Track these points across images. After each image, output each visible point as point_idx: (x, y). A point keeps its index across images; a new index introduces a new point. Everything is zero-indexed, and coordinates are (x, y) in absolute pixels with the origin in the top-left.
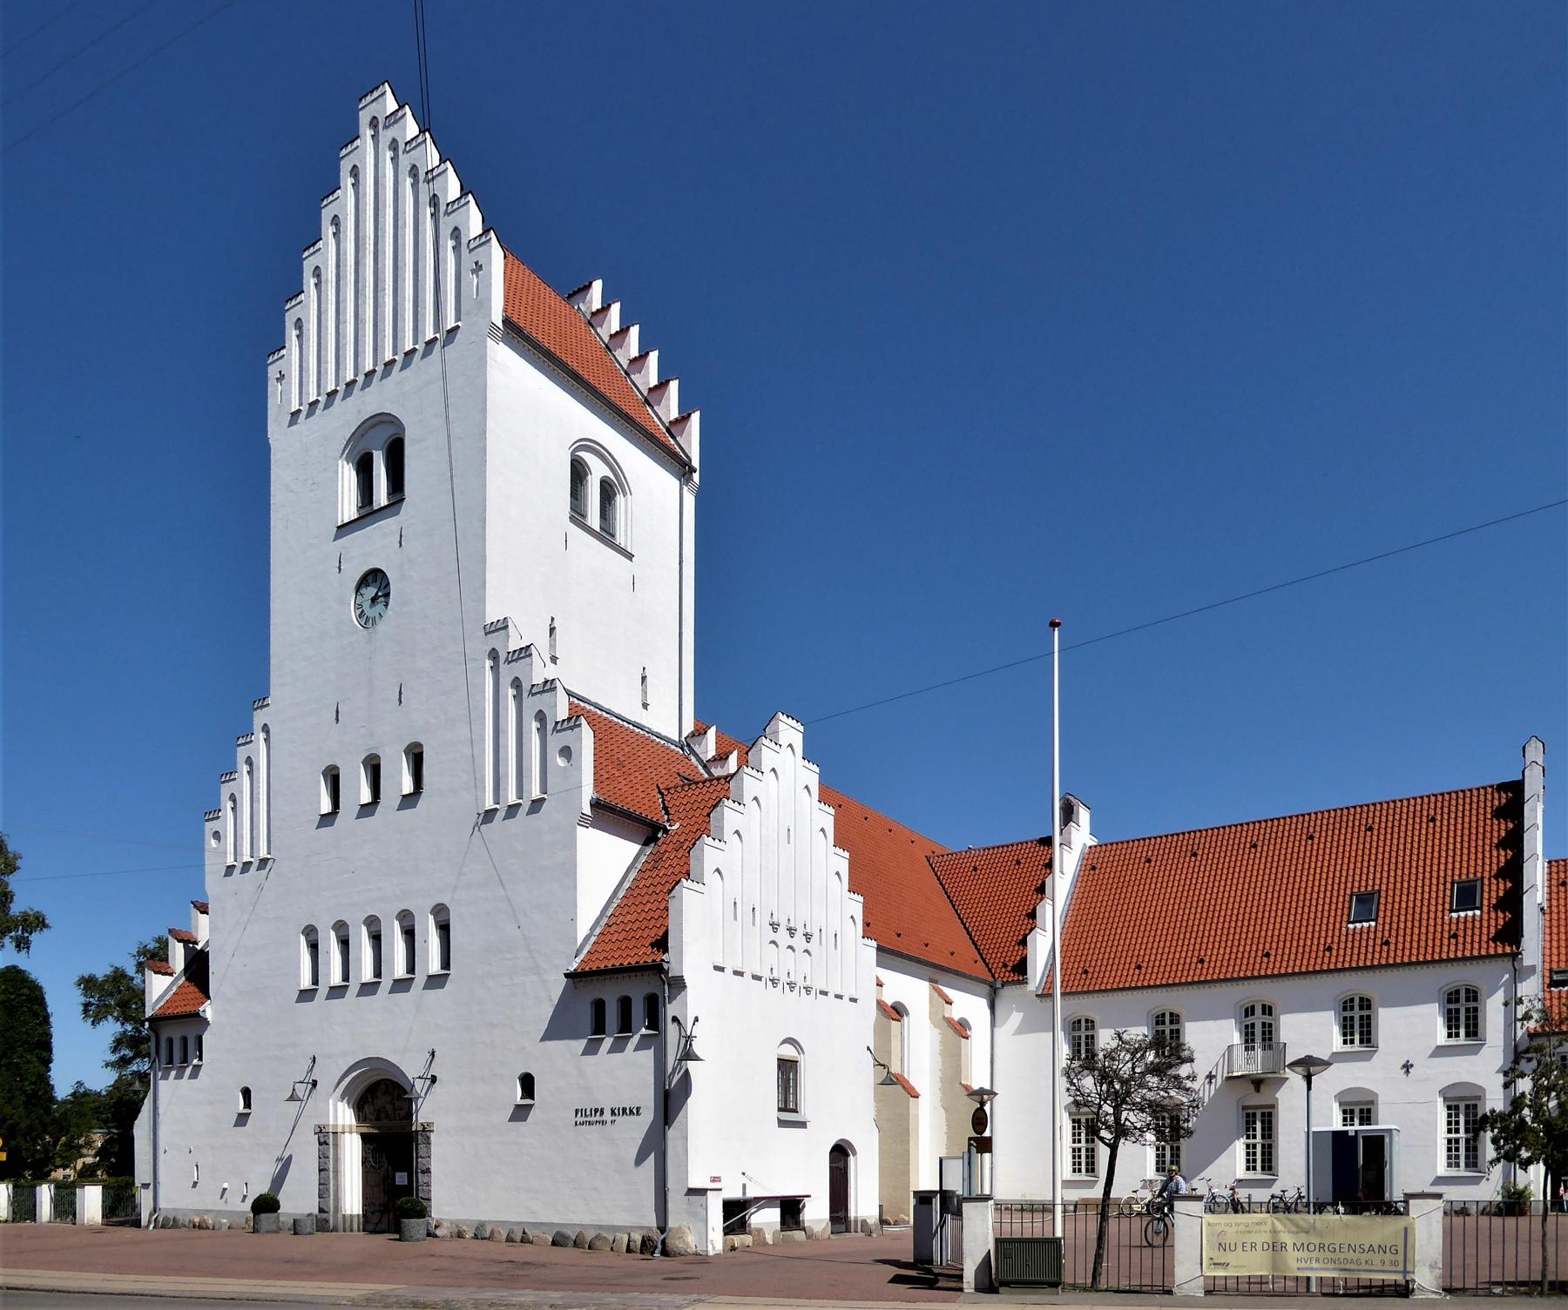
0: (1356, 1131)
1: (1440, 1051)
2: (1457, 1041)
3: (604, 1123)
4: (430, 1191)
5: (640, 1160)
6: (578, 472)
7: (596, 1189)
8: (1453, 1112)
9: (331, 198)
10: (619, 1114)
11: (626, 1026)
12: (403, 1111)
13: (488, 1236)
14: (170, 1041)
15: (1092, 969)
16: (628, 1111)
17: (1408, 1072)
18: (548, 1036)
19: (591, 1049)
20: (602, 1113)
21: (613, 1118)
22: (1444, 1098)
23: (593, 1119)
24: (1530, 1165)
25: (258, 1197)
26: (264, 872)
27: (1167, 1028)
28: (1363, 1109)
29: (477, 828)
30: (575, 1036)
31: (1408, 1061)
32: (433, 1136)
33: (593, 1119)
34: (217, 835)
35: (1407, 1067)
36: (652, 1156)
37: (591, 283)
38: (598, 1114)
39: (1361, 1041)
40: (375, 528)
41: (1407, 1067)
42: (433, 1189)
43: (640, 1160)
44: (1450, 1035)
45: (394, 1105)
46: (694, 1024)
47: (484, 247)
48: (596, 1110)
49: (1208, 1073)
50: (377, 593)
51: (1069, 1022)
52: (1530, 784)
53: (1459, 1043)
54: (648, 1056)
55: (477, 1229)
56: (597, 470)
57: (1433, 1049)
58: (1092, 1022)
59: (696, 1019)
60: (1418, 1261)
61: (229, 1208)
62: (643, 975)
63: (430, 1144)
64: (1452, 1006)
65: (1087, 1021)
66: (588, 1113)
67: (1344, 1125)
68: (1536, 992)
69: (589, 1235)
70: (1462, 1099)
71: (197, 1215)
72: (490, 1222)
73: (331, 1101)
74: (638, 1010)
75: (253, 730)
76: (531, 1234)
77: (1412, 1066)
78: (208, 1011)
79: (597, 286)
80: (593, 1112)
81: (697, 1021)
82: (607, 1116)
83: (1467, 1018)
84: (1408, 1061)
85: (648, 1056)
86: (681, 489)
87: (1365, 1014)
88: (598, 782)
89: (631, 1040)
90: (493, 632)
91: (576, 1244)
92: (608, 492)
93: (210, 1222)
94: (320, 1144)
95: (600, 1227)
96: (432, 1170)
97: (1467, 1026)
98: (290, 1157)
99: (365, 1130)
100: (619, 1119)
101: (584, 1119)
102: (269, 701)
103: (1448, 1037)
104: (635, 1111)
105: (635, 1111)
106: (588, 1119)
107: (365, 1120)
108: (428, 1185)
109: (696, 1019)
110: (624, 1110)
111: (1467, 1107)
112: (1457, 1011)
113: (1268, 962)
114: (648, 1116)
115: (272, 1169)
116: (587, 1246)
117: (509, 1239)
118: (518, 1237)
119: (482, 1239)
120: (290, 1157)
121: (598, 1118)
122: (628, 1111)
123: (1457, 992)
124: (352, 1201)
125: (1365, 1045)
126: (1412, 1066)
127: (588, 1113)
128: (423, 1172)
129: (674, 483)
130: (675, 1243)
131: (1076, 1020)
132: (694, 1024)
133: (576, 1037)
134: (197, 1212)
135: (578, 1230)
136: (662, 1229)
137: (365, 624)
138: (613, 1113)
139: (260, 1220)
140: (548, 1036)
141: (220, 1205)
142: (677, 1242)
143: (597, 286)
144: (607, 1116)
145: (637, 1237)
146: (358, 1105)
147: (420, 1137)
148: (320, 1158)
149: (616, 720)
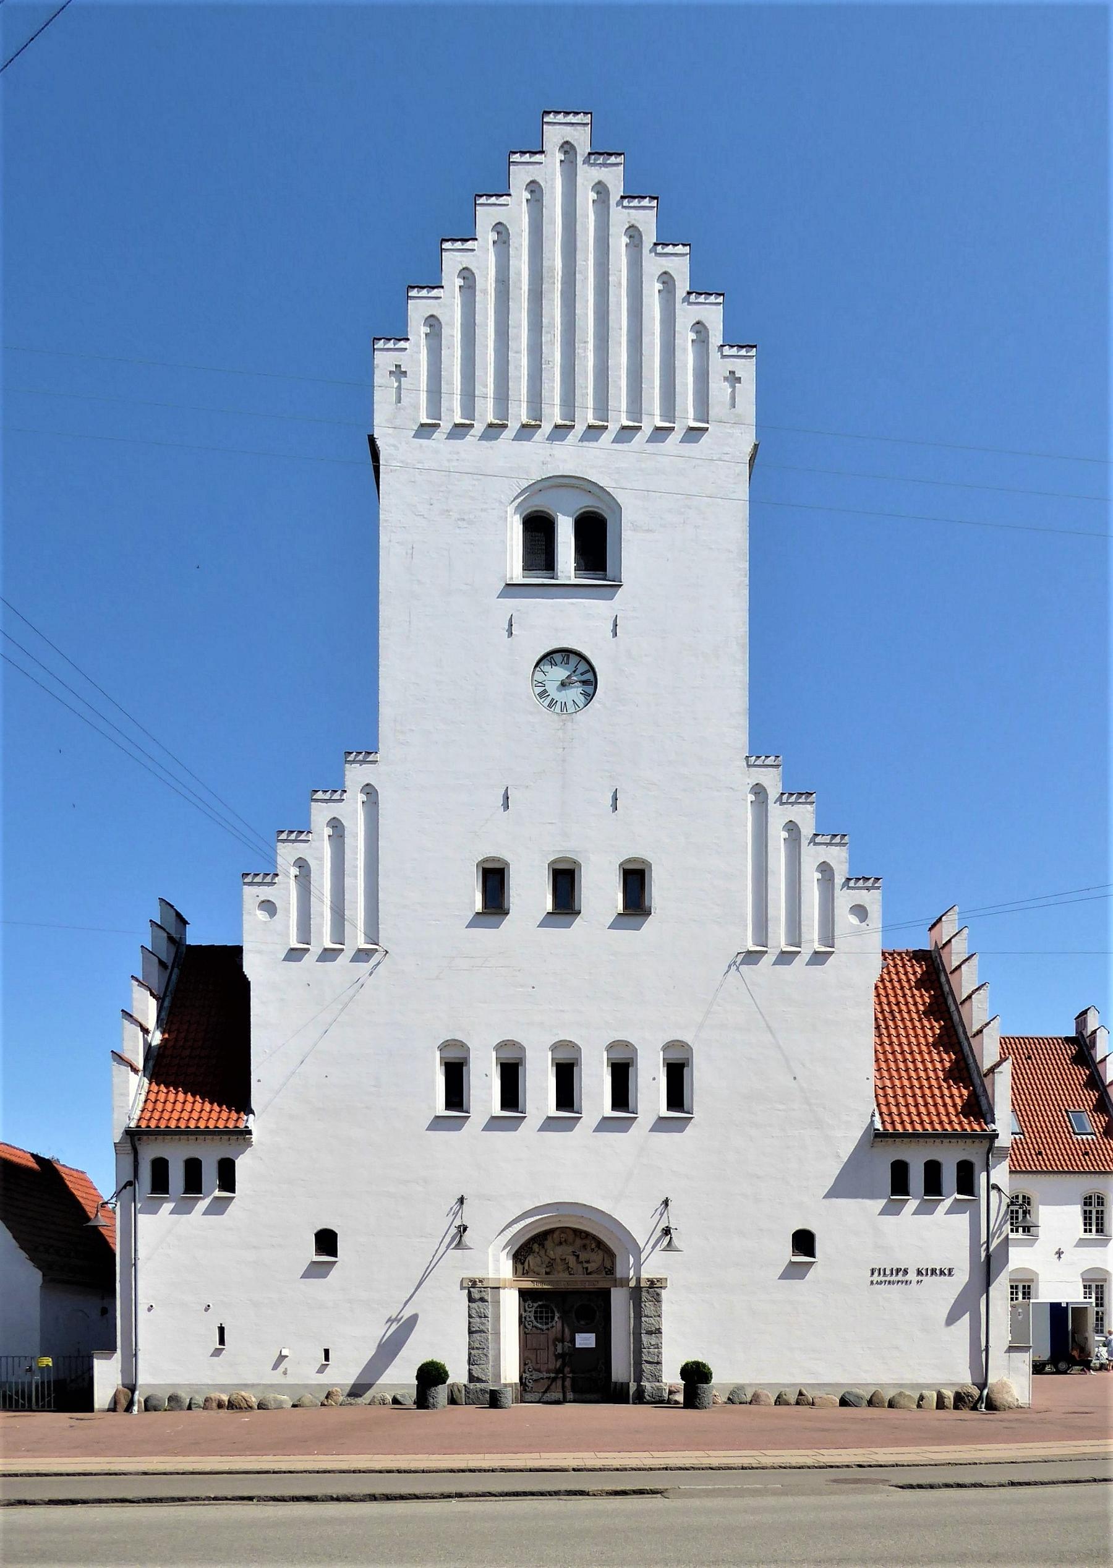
0: (1067, 1303)
1: (1082, 1243)
2: (1016, 1235)
4: (660, 1353)
5: (951, 1319)
7: (897, 1348)
8: (1087, 1290)
9: (493, 200)
10: (927, 1274)
11: (933, 1187)
12: (593, 1264)
13: (749, 1400)
16: (938, 1272)
17: (1060, 1257)
18: (834, 1192)
19: (894, 1209)
20: (906, 1272)
21: (920, 1278)
22: (1083, 1279)
23: (894, 1278)
25: (421, 1366)
26: (365, 967)
28: (1025, 1286)
29: (734, 968)
30: (873, 1196)
31: (1060, 1249)
32: (664, 1294)
33: (894, 1278)
34: (269, 907)
35: (1059, 1254)
36: (967, 1315)
38: (901, 1274)
39: (1097, 1231)
40: (573, 604)
41: (1059, 1254)
42: (664, 1350)
43: (951, 1319)
44: (1085, 1231)
47: (743, 360)
48: (898, 1271)
49: (1057, 1250)
50: (569, 677)
52: (1101, 1043)
53: (1017, 1237)
54: (962, 1220)
55: (731, 1394)
57: (1077, 1240)
58: (1029, 1198)
61: (290, 1380)
62: (974, 1142)
63: (659, 1301)
64: (1088, 1208)
66: (888, 1272)
67: (1085, 1298)
69: (888, 1394)
70: (1021, 1281)
71: (223, 1392)
72: (750, 1385)
73: (490, 1250)
74: (949, 1177)
75: (343, 783)
76: (809, 1394)
77: (1063, 1252)
78: (252, 1125)
80: (894, 1272)
82: (912, 1276)
83: (1097, 1218)
84: (1060, 1249)
85: (962, 1220)
87: (1100, 1209)
89: (942, 1203)
90: (759, 766)
91: (870, 1403)
93: (254, 1399)
94: (471, 1299)
95: (901, 1385)
96: (663, 1331)
97: (1097, 1225)
98: (414, 1318)
99: (527, 1285)
100: (927, 1280)
101: (882, 1278)
102: (378, 757)
103: (1085, 1232)
104: (946, 1272)
105: (946, 1272)
106: (888, 1279)
107: (525, 1273)
108: (658, 1346)
110: (933, 1271)
111: (1097, 1286)
112: (1090, 1212)
114: (962, 1277)
115: (378, 1331)
116: (886, 1405)
117: (780, 1401)
118: (793, 1398)
119: (741, 1403)
120: (414, 1318)
121: (900, 1277)
122: (938, 1272)
123: (1090, 1197)
124: (510, 1371)
125: (1026, 1233)
126: (1063, 1252)
127: (888, 1272)
128: (650, 1333)
130: (1000, 1398)
133: (872, 1196)
134: (222, 1388)
135: (873, 1390)
136: (982, 1386)
137: (579, 707)
138: (919, 1272)
139: (437, 1393)
140: (834, 1192)
141: (276, 1378)
142: (1006, 1396)
144: (912, 1276)
145: (949, 1394)
147: (644, 1294)
148: (470, 1316)
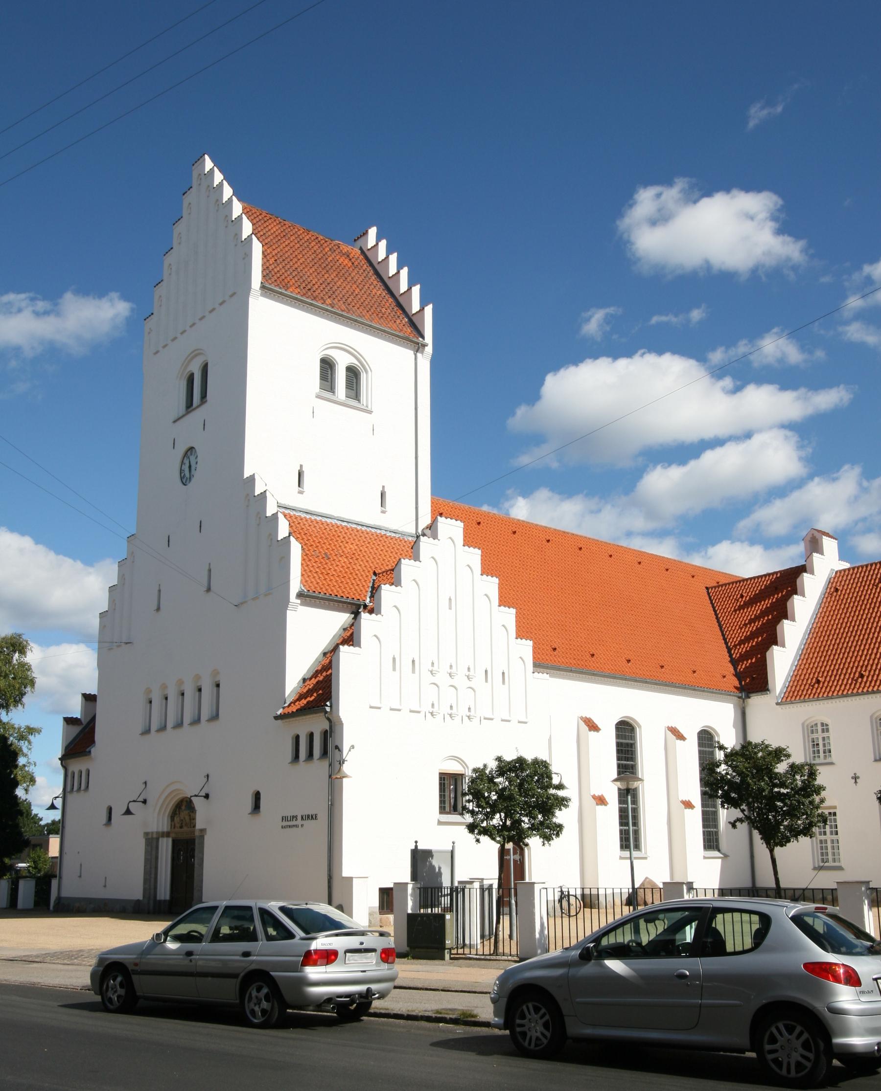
3: (296, 826)
6: (327, 366)
14: (74, 773)
15: (867, 672)
17: (856, 782)
21: (303, 822)
24: (20, 834)
27: (820, 735)
35: (855, 778)
37: (367, 231)
43: (440, 868)
45: (190, 815)
46: (350, 750)
51: (876, 718)
56: (342, 362)
58: (827, 725)
59: (353, 747)
60: (736, 921)
65: (822, 724)
68: (82, 792)
79: (373, 232)
81: (353, 748)
86: (416, 355)
88: (304, 581)
92: (353, 374)
105: (314, 817)
109: (353, 747)
110: (308, 816)
113: (818, 687)
127: (289, 819)
129: (410, 353)
131: (813, 724)
132: (350, 750)
143: (373, 232)
146: (171, 817)
149: (354, 526)
